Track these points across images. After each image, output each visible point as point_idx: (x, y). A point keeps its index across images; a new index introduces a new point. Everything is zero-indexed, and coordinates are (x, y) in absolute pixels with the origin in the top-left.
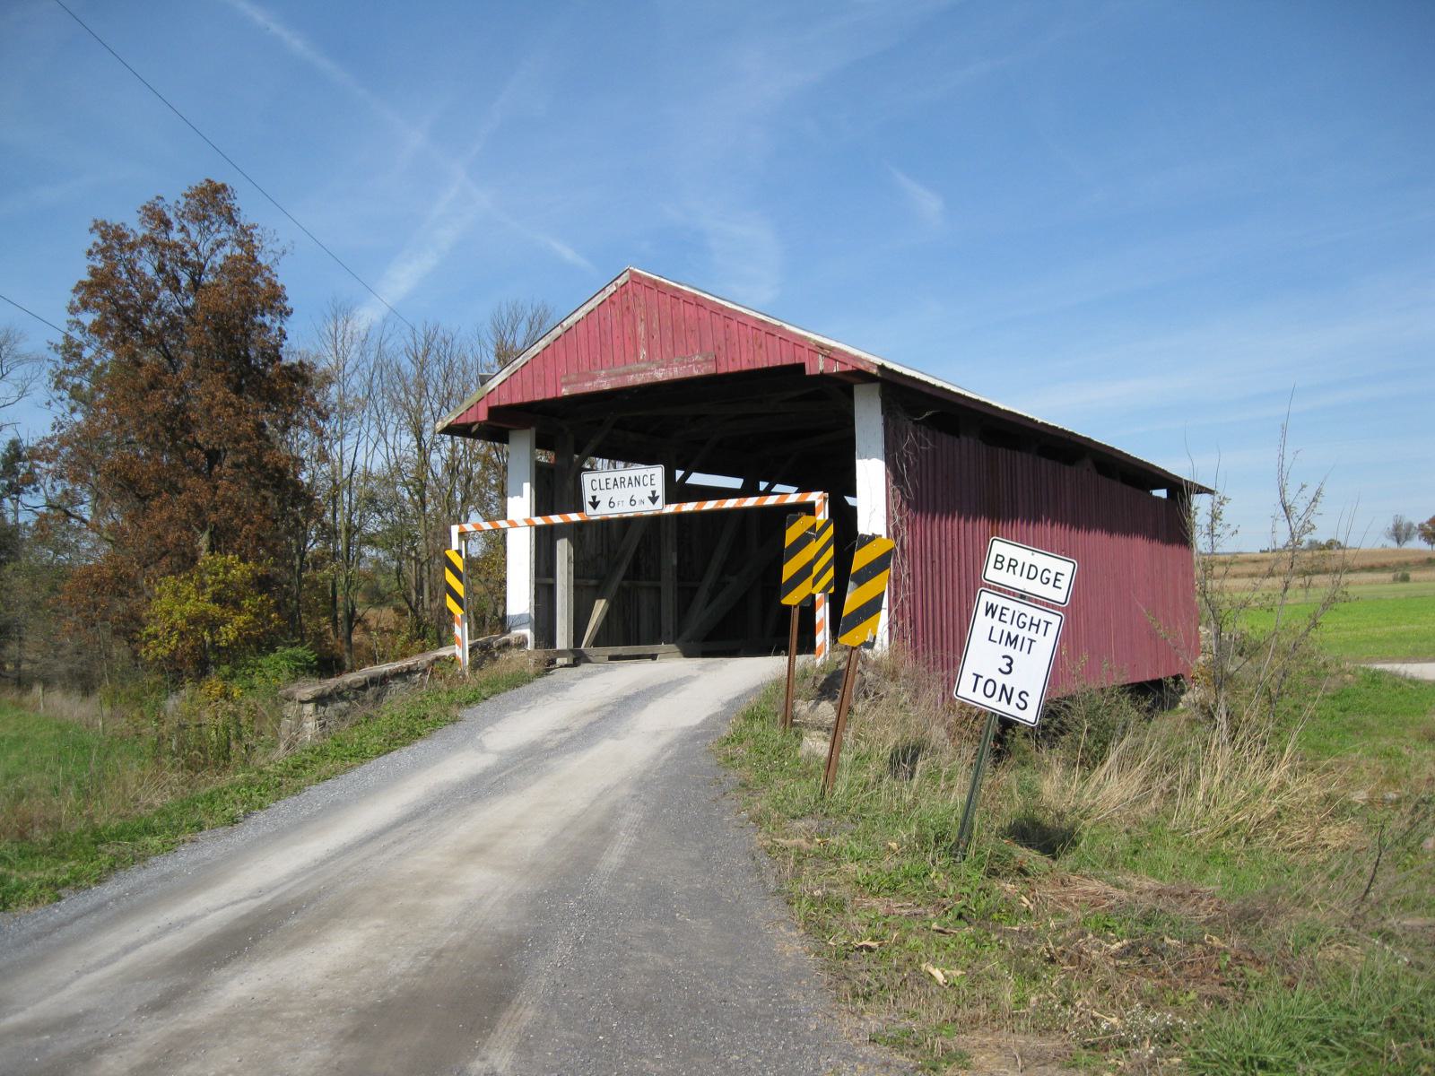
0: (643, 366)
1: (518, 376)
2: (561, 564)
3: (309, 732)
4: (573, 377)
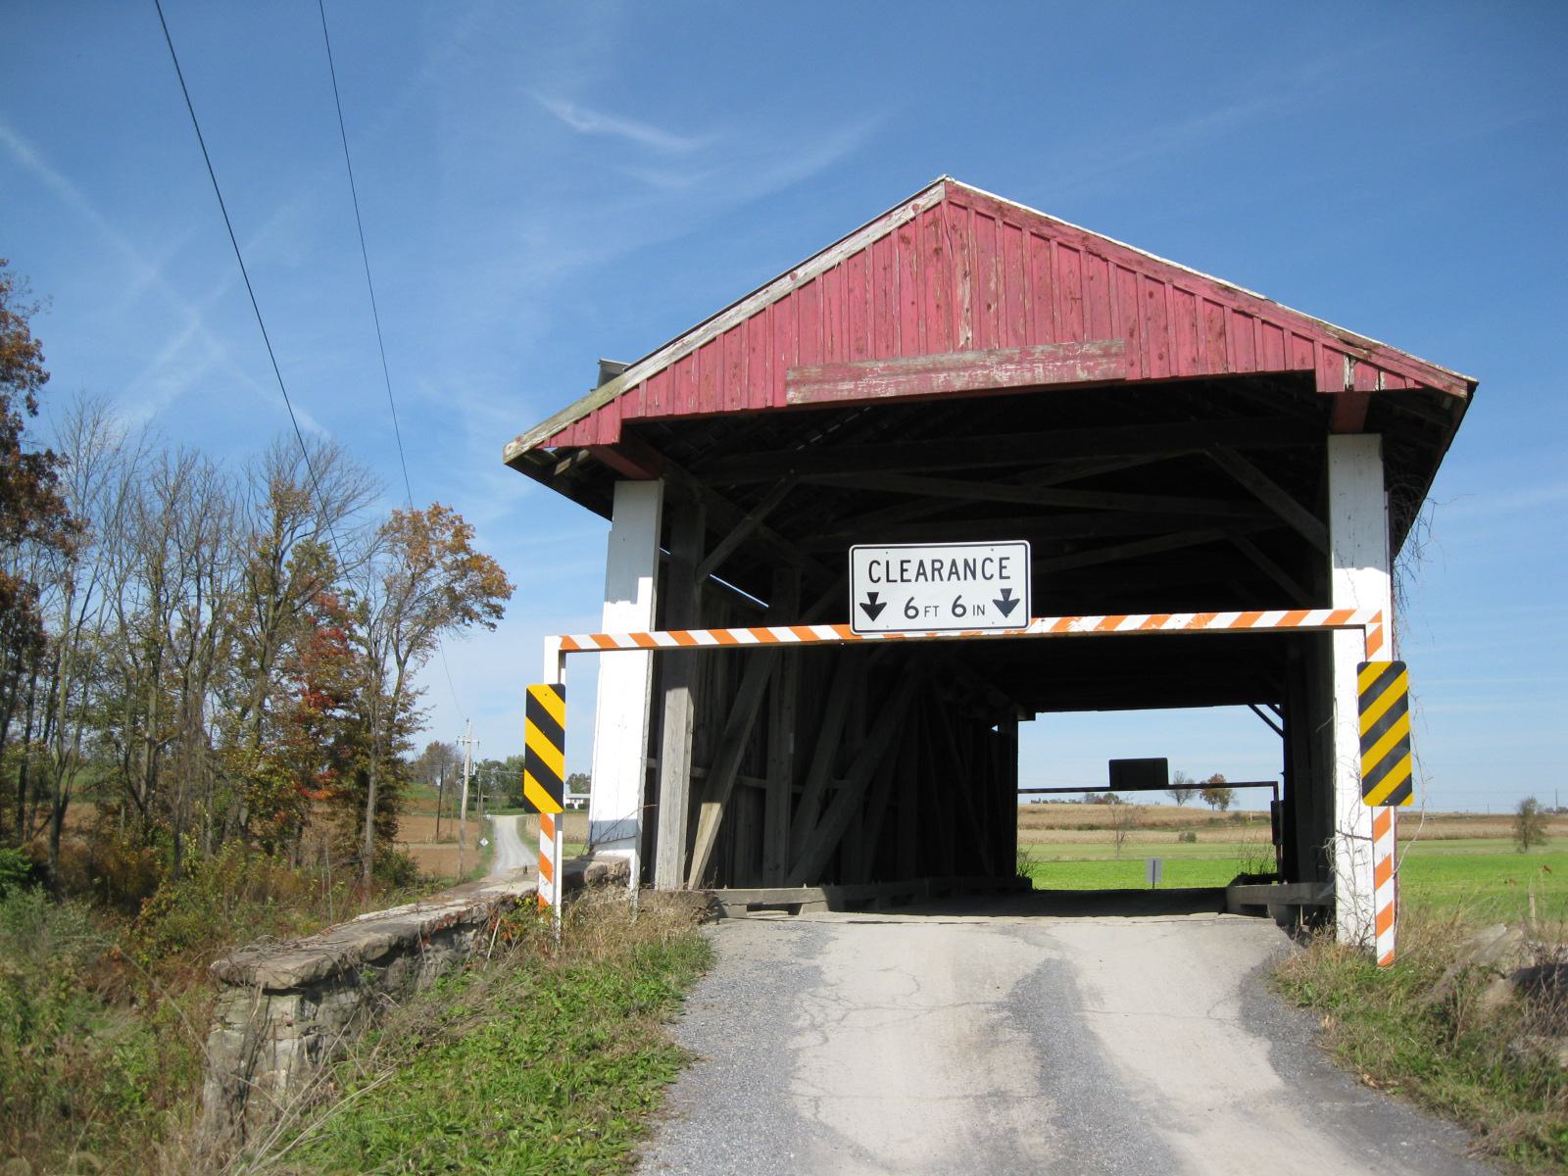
0: (969, 356)
1: (693, 364)
2: (674, 733)
3: (283, 1060)
4: (814, 371)
